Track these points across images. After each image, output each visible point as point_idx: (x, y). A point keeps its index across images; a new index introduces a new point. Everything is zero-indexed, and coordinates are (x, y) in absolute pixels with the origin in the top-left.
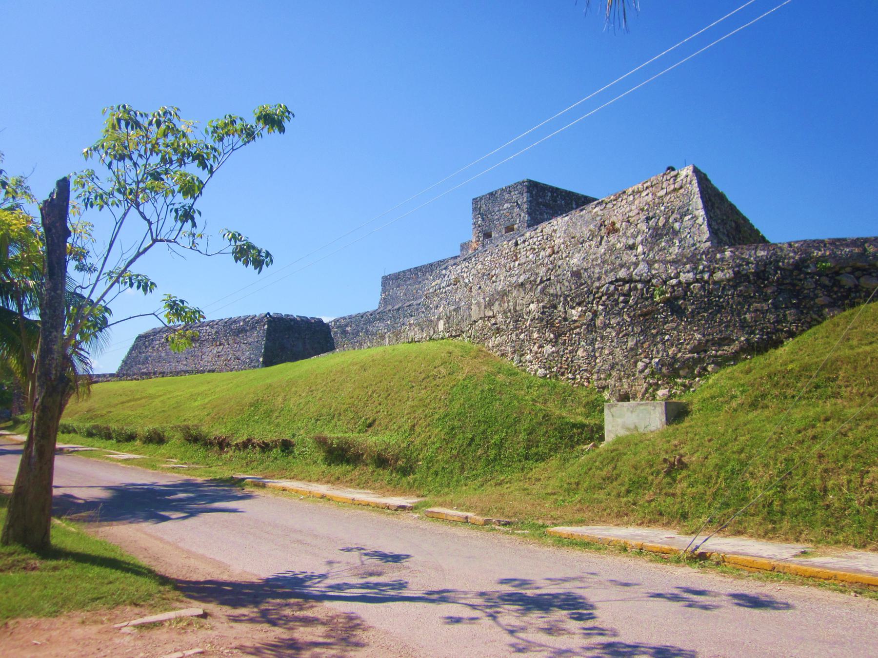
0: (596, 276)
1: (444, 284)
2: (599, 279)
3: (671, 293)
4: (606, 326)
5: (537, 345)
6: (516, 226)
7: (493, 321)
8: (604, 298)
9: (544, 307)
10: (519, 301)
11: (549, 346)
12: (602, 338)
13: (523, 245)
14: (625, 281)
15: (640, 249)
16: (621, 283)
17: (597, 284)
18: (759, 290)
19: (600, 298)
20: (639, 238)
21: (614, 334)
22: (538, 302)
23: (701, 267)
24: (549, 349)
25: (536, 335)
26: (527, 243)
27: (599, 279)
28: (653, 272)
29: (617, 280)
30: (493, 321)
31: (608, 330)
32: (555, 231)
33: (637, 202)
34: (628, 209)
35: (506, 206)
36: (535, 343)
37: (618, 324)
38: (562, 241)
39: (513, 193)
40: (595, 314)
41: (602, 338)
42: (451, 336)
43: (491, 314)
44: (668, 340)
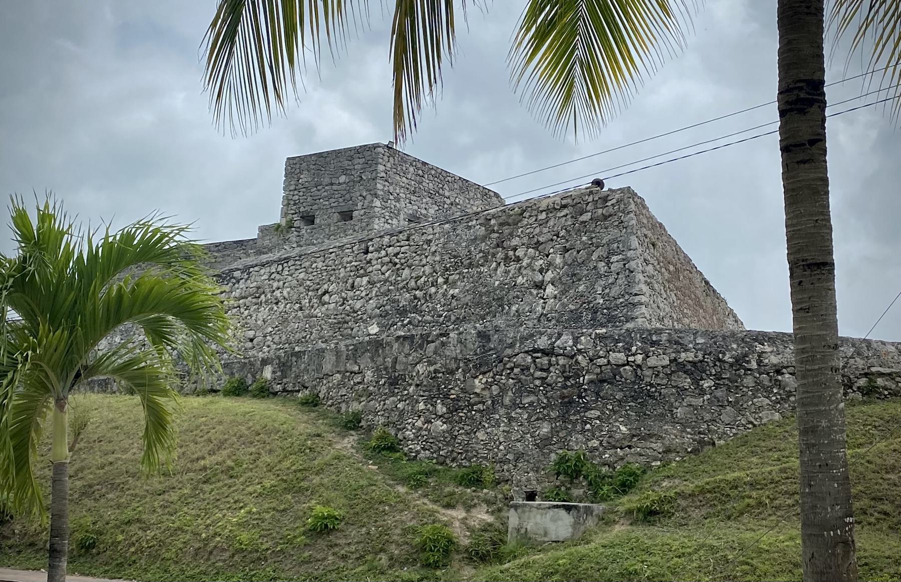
0: (509, 341)
1: (236, 293)
2: (512, 346)
3: (566, 285)
4: (515, 405)
5: (422, 419)
6: (355, 214)
7: (358, 379)
8: (516, 370)
9: (436, 371)
10: (401, 358)
11: (439, 423)
12: (510, 419)
13: (376, 255)
14: (545, 352)
15: (550, 290)
16: (539, 355)
17: (509, 351)
18: (696, 382)
19: (512, 369)
20: (549, 275)
21: (525, 416)
22: (430, 363)
23: (634, 349)
24: (440, 426)
25: (421, 406)
26: (383, 253)
27: (512, 346)
28: (579, 347)
29: (535, 351)
30: (358, 379)
31: (519, 410)
32: (429, 242)
33: (551, 223)
34: (538, 230)
35: (343, 179)
36: (419, 417)
37: (531, 404)
38: (438, 258)
39: (356, 161)
40: (503, 390)
41: (510, 419)
42: (284, 390)
43: (356, 368)
44: (588, 430)
